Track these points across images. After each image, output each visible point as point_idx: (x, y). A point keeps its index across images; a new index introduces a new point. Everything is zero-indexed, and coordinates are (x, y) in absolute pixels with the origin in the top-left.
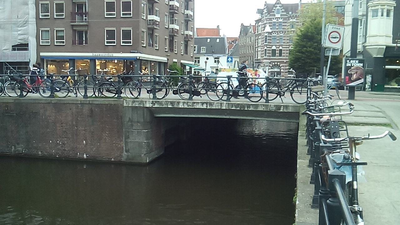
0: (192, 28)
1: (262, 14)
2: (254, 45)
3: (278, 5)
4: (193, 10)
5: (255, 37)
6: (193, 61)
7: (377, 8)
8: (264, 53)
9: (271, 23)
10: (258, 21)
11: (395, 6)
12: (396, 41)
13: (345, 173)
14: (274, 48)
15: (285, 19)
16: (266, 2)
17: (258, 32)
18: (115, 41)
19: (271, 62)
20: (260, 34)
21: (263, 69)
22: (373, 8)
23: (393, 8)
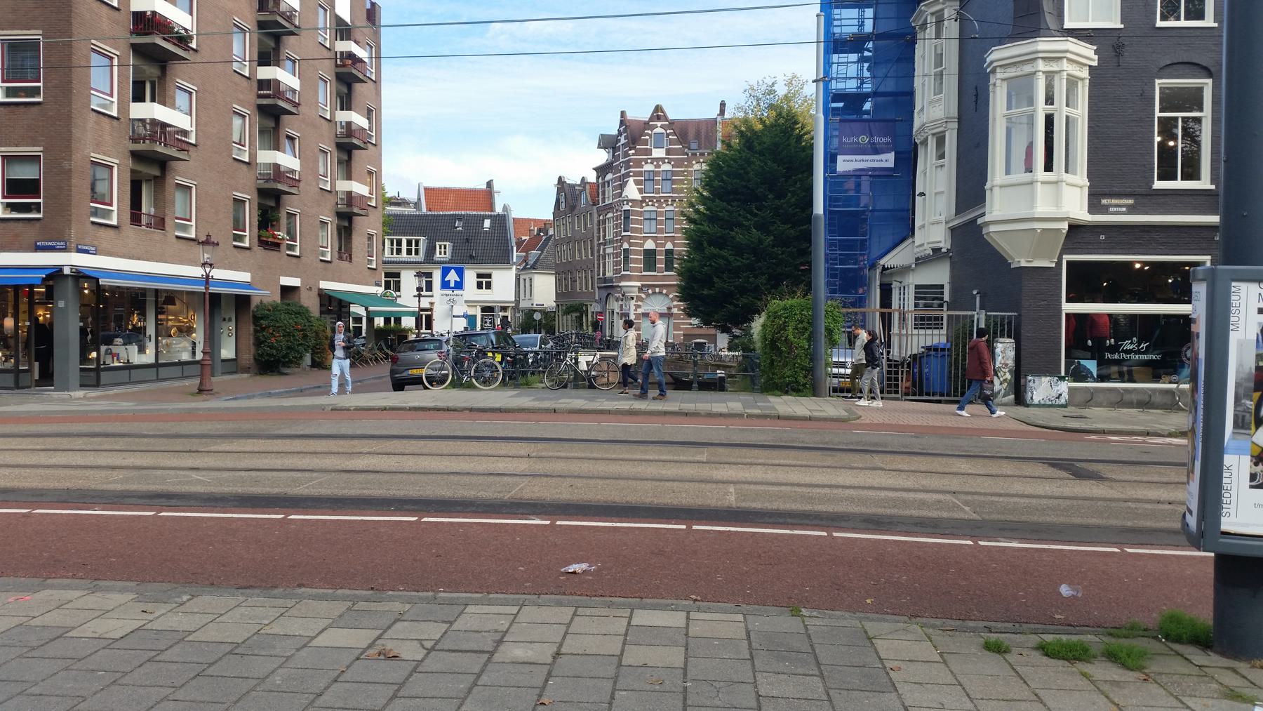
0: (370, 173)
1: (615, 149)
2: (596, 238)
3: (659, 124)
4: (371, 113)
5: (595, 215)
6: (378, 285)
7: (1027, 69)
8: (621, 261)
9: (640, 174)
10: (602, 170)
11: (1095, 64)
12: (1104, 201)
13: (777, 408)
14: (650, 245)
15: (678, 163)
16: (623, 114)
17: (604, 201)
19: (643, 285)
20: (610, 207)
21: (622, 305)
22: (1011, 73)
23: (1085, 74)
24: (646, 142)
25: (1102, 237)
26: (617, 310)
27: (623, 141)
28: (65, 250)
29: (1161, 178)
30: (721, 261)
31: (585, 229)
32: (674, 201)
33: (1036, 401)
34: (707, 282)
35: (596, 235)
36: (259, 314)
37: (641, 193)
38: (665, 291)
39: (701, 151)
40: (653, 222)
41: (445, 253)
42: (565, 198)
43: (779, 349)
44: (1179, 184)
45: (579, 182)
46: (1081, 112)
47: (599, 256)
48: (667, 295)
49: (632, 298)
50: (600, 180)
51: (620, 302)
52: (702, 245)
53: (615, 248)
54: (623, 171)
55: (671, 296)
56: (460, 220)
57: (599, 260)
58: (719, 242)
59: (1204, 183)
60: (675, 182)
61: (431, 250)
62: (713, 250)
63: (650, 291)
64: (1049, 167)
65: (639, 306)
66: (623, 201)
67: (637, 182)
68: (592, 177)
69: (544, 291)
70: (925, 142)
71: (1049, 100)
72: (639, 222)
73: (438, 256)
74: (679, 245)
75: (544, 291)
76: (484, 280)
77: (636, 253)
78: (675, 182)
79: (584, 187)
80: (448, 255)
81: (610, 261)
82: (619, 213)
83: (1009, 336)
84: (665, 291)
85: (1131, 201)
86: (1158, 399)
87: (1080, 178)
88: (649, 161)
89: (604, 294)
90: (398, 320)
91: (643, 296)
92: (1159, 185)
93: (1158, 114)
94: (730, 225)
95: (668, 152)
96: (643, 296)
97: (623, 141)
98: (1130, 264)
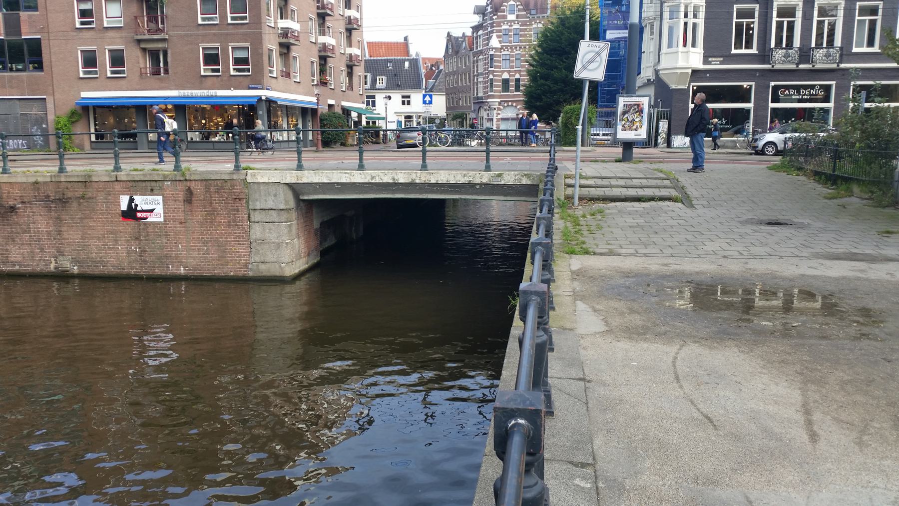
1: (484, 15)
2: (472, 72)
5: (472, 57)
6: (363, 103)
9: (500, 31)
10: (476, 29)
12: (710, 59)
14: (506, 76)
17: (477, 48)
18: (220, 67)
19: (501, 101)
20: (481, 52)
21: (488, 114)
24: (503, 11)
25: (708, 75)
26: (485, 117)
27: (489, 10)
28: (262, 89)
29: (736, 48)
30: (546, 87)
31: (465, 66)
32: (520, 48)
33: (675, 146)
34: (539, 98)
35: (472, 70)
36: (322, 118)
37: (500, 43)
38: (514, 104)
39: (538, 15)
40: (508, 61)
41: (382, 83)
42: (452, 46)
43: (568, 127)
44: (744, 51)
45: (461, 35)
46: (701, 21)
47: (474, 83)
48: (516, 107)
49: (495, 109)
50: (475, 35)
51: (487, 112)
52: (537, 78)
53: (484, 78)
54: (489, 29)
55: (518, 107)
56: (390, 62)
57: (474, 86)
58: (545, 77)
59: (754, 51)
60: (521, 36)
61: (374, 82)
62: (542, 81)
63: (506, 105)
64: (685, 45)
65: (499, 114)
66: (489, 49)
67: (498, 37)
68: (469, 33)
69: (439, 106)
70: (646, 26)
71: (686, 16)
72: (499, 62)
73: (378, 85)
74: (523, 75)
75: (439, 106)
76: (406, 100)
77: (497, 81)
78: (521, 36)
79: (465, 39)
80: (384, 85)
81: (481, 86)
82: (487, 56)
83: (667, 119)
84: (514, 104)
85: (721, 59)
86: (730, 144)
87: (700, 49)
88: (506, 23)
89: (477, 106)
90: (374, 123)
91: (502, 107)
92: (734, 51)
93: (735, 20)
94: (552, 68)
95: (518, 17)
96: (502, 107)
97: (489, 10)
98: (742, 86)
